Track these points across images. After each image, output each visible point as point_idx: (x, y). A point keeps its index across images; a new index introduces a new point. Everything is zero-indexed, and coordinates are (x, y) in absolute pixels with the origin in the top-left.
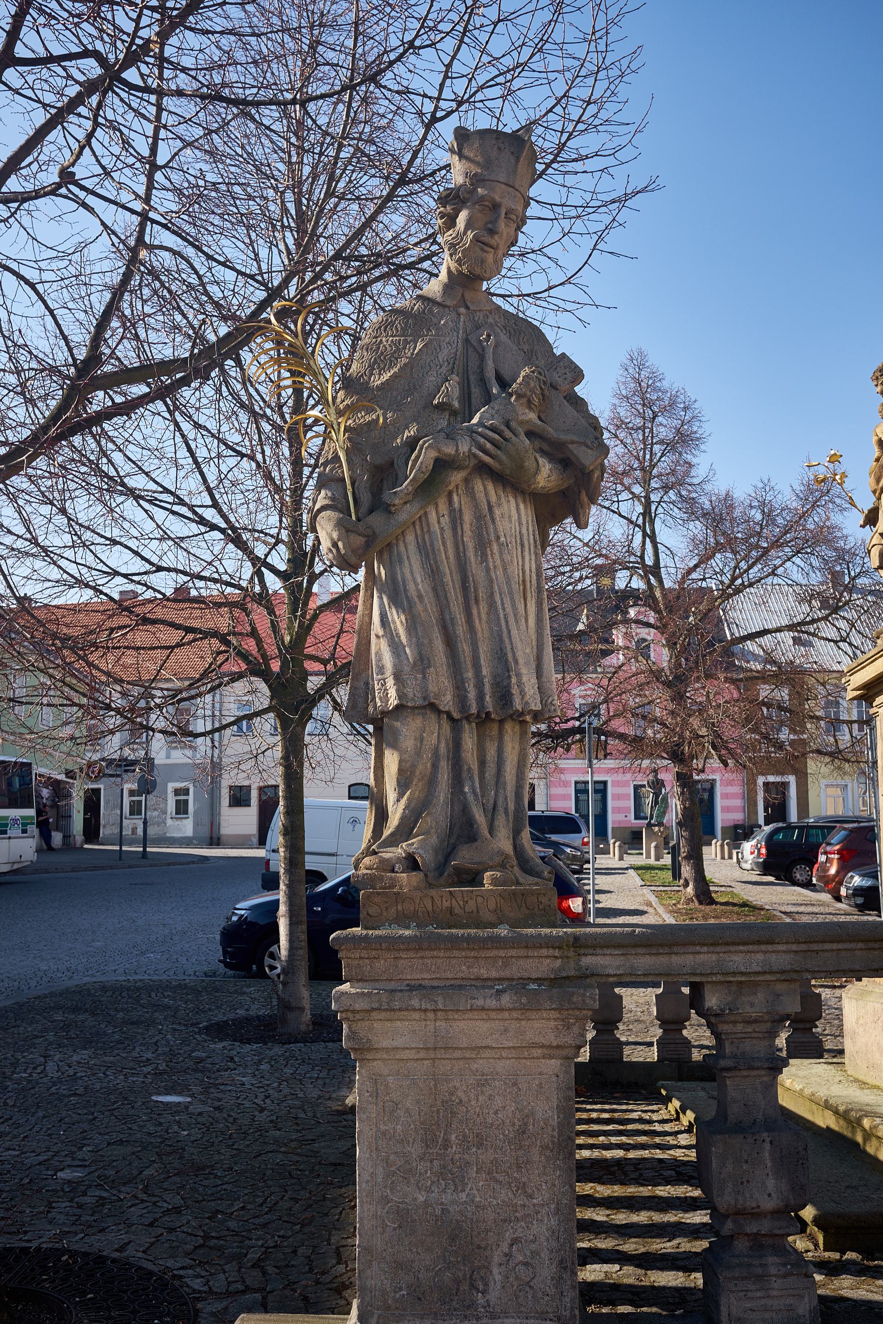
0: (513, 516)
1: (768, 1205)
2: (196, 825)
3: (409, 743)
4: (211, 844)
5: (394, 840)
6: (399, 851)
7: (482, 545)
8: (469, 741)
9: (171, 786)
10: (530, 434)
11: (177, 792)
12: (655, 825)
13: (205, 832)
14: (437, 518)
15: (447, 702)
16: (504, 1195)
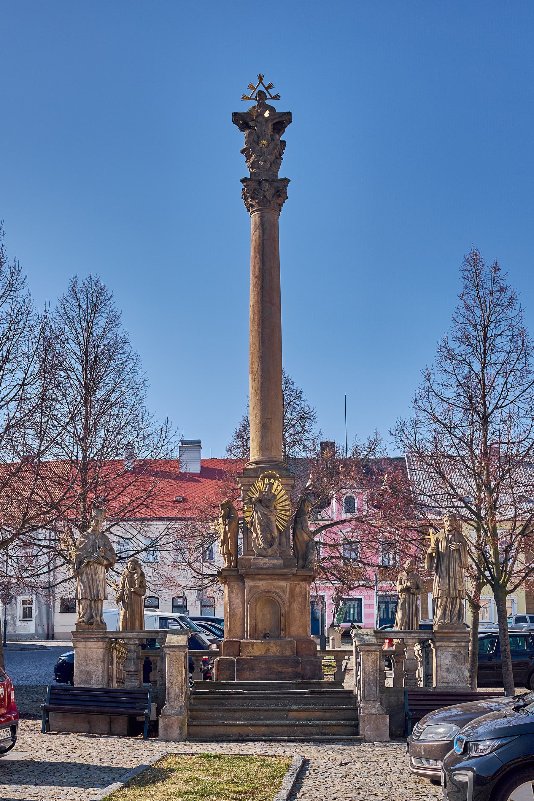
0: (101, 569)
1: (133, 670)
2: (37, 625)
3: (83, 604)
4: (48, 639)
5: (81, 618)
6: (82, 620)
7: (95, 574)
8: (93, 603)
9: (20, 599)
10: (102, 557)
11: (24, 602)
12: (336, 626)
13: (43, 630)
14: (88, 569)
15: (89, 598)
16: (95, 668)
